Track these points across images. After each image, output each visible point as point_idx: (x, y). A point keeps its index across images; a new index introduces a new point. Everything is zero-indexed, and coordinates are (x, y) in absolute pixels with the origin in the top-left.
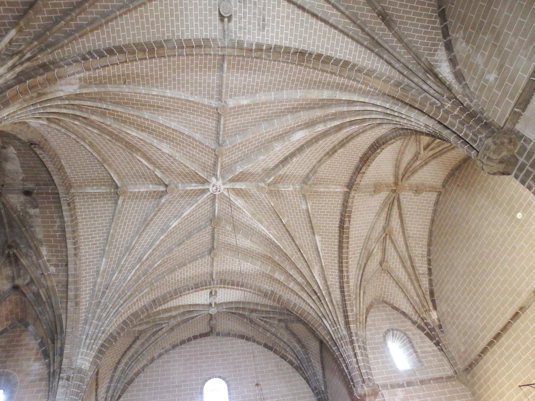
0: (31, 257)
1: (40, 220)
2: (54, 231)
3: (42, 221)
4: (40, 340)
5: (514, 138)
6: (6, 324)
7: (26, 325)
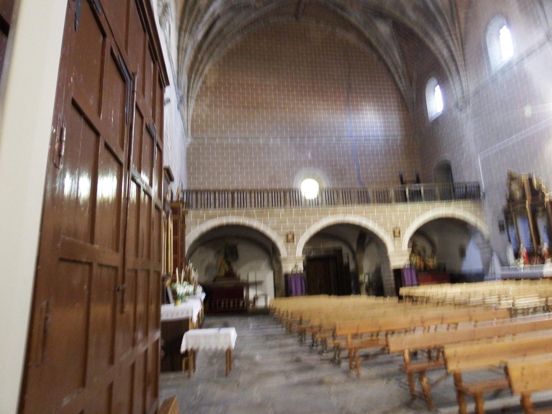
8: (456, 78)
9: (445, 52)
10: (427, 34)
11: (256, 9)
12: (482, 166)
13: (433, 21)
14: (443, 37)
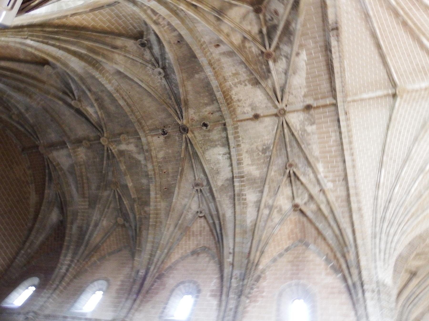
0: (309, 175)
1: (316, 136)
2: (330, 147)
3: (318, 138)
4: (325, 257)
5: (344, 217)
6: (289, 243)
7: (307, 245)
8: (51, 291)
9: (63, 270)
10: (68, 248)
11: (11, 117)
12: (65, 37)
13: (78, 245)
14: (73, 257)
